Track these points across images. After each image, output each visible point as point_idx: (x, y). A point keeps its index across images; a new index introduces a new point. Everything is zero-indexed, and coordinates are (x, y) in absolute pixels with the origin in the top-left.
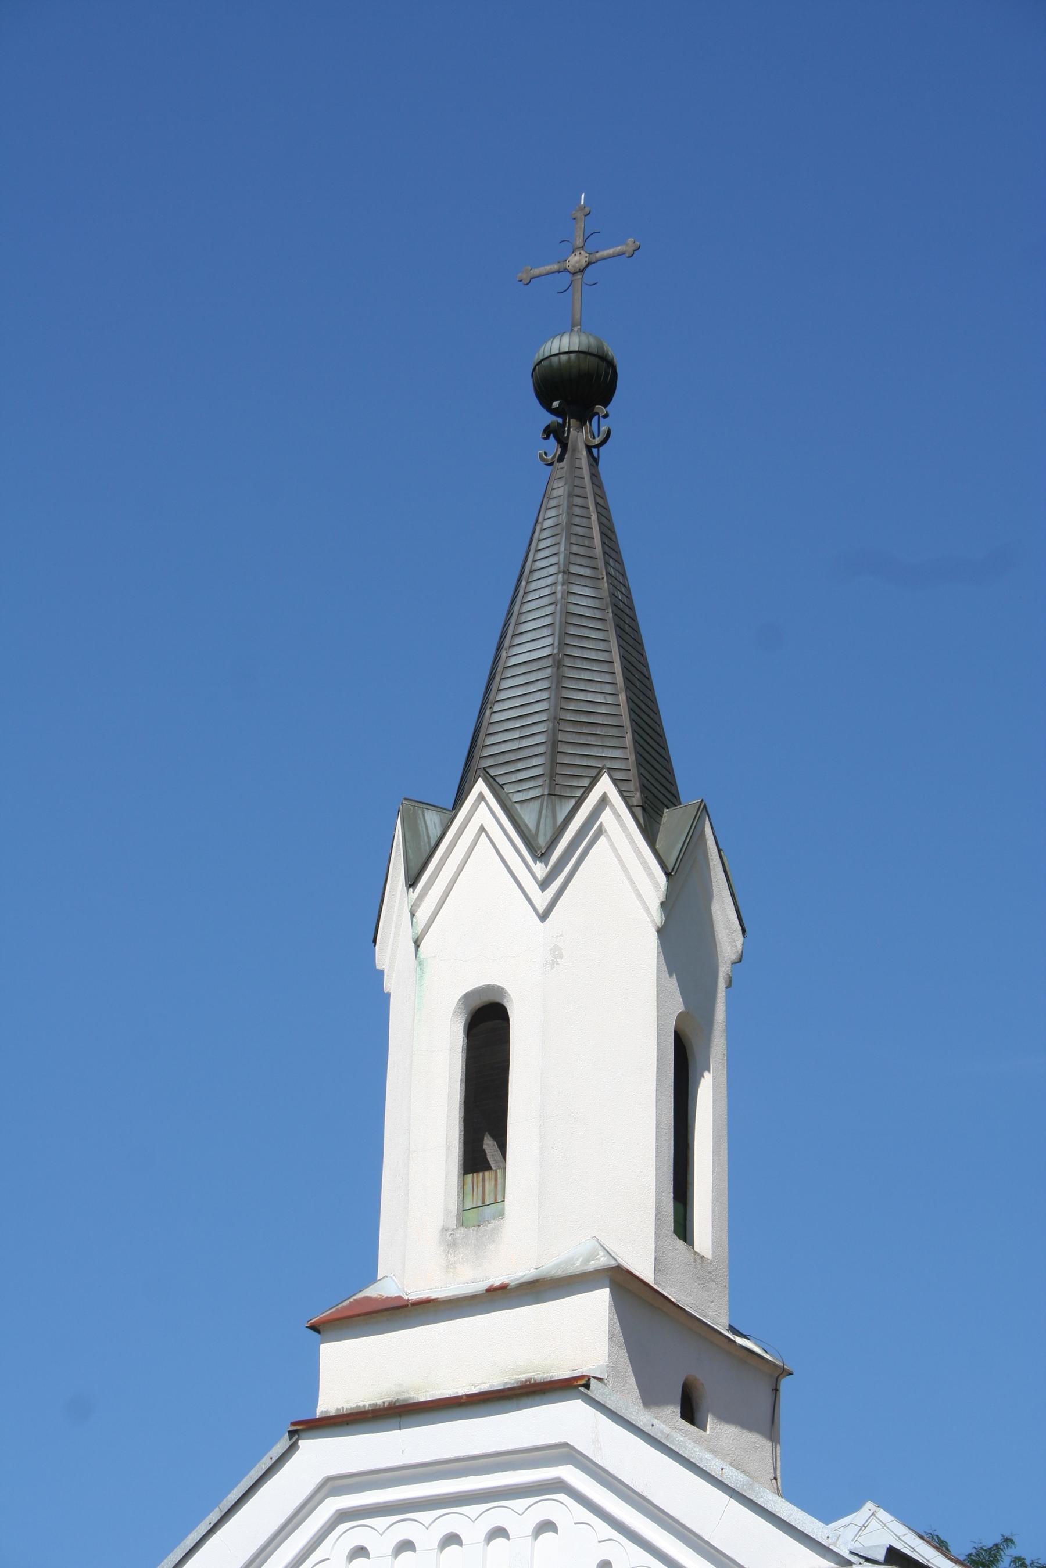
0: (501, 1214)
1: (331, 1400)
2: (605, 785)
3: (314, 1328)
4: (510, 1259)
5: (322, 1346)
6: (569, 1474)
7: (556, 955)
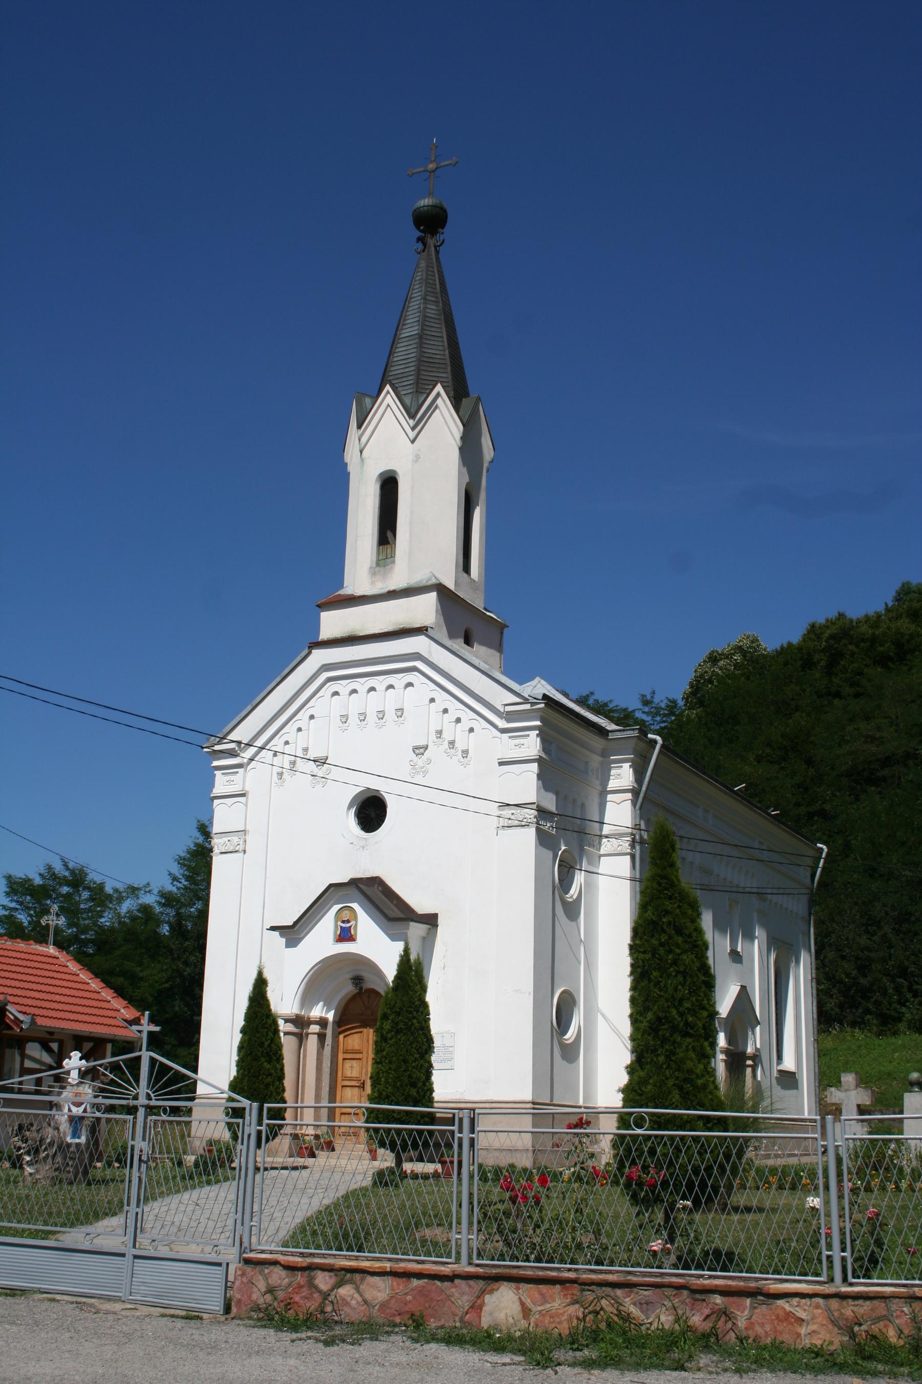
0: (394, 562)
1: (325, 633)
2: (439, 388)
3: (318, 606)
7: (417, 458)
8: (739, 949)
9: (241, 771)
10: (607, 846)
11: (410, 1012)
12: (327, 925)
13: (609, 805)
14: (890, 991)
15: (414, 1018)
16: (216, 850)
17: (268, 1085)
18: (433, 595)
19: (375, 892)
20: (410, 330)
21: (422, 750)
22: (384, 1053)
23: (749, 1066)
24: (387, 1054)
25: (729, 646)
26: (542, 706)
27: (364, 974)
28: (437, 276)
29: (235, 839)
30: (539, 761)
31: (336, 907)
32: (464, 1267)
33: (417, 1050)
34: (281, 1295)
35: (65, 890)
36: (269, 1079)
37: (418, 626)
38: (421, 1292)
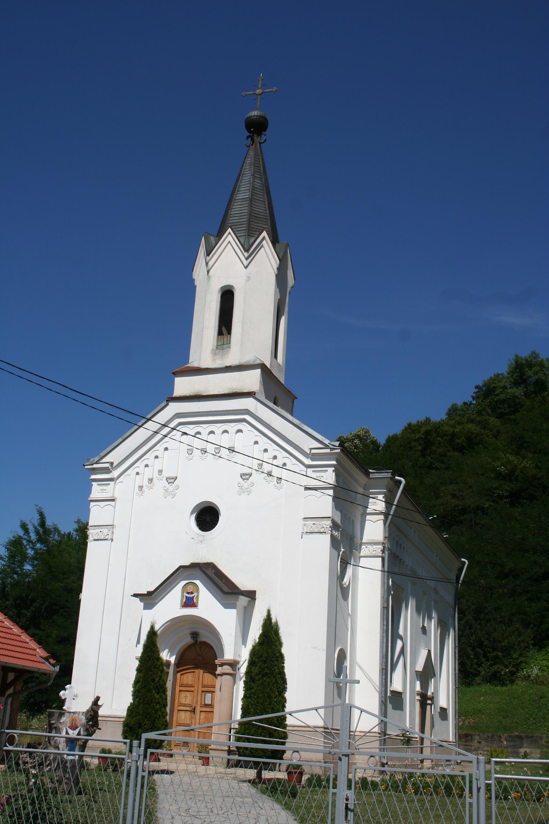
0: (229, 347)
1: (177, 393)
2: (264, 234)
3: (174, 373)
5: (176, 379)
7: (249, 279)
8: (425, 625)
9: (112, 483)
10: (365, 550)
11: (273, 661)
12: (176, 595)
13: (367, 523)
14: (472, 656)
15: (276, 665)
16: (90, 538)
17: (157, 711)
18: (258, 371)
19: (210, 572)
20: (243, 194)
21: (247, 477)
22: (253, 691)
23: (429, 704)
24: (256, 691)
25: (351, 434)
26: (339, 451)
27: (201, 631)
28: (261, 162)
29: (105, 531)
31: (183, 583)
33: (277, 689)
36: (158, 707)
37: (247, 391)
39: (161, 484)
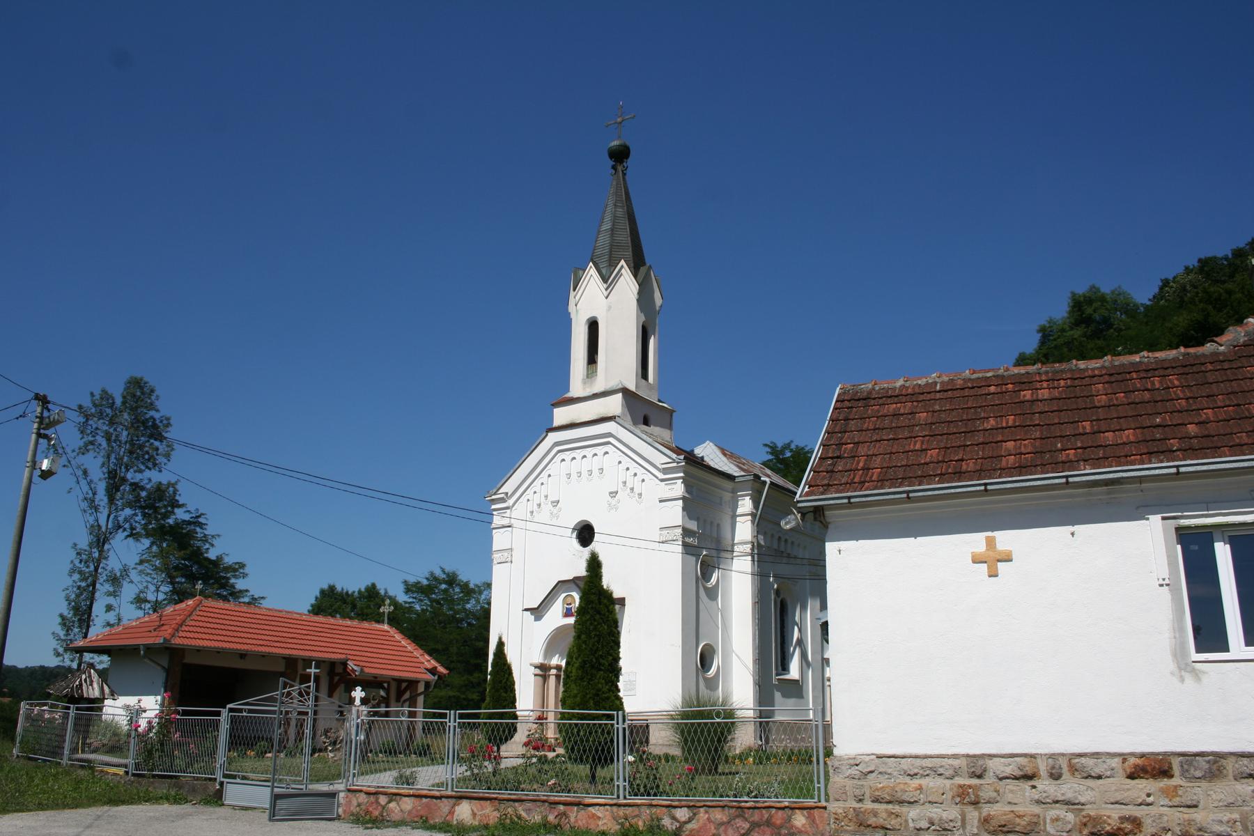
1: (556, 423)
2: (622, 262)
4: (598, 387)
6: (611, 440)
7: (610, 308)
30: (684, 499)
31: (564, 595)
32: (449, 793)
34: (363, 807)
35: (443, 586)
38: (427, 805)
39: (547, 507)
